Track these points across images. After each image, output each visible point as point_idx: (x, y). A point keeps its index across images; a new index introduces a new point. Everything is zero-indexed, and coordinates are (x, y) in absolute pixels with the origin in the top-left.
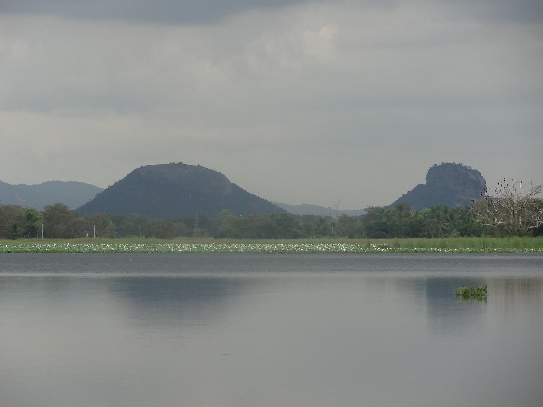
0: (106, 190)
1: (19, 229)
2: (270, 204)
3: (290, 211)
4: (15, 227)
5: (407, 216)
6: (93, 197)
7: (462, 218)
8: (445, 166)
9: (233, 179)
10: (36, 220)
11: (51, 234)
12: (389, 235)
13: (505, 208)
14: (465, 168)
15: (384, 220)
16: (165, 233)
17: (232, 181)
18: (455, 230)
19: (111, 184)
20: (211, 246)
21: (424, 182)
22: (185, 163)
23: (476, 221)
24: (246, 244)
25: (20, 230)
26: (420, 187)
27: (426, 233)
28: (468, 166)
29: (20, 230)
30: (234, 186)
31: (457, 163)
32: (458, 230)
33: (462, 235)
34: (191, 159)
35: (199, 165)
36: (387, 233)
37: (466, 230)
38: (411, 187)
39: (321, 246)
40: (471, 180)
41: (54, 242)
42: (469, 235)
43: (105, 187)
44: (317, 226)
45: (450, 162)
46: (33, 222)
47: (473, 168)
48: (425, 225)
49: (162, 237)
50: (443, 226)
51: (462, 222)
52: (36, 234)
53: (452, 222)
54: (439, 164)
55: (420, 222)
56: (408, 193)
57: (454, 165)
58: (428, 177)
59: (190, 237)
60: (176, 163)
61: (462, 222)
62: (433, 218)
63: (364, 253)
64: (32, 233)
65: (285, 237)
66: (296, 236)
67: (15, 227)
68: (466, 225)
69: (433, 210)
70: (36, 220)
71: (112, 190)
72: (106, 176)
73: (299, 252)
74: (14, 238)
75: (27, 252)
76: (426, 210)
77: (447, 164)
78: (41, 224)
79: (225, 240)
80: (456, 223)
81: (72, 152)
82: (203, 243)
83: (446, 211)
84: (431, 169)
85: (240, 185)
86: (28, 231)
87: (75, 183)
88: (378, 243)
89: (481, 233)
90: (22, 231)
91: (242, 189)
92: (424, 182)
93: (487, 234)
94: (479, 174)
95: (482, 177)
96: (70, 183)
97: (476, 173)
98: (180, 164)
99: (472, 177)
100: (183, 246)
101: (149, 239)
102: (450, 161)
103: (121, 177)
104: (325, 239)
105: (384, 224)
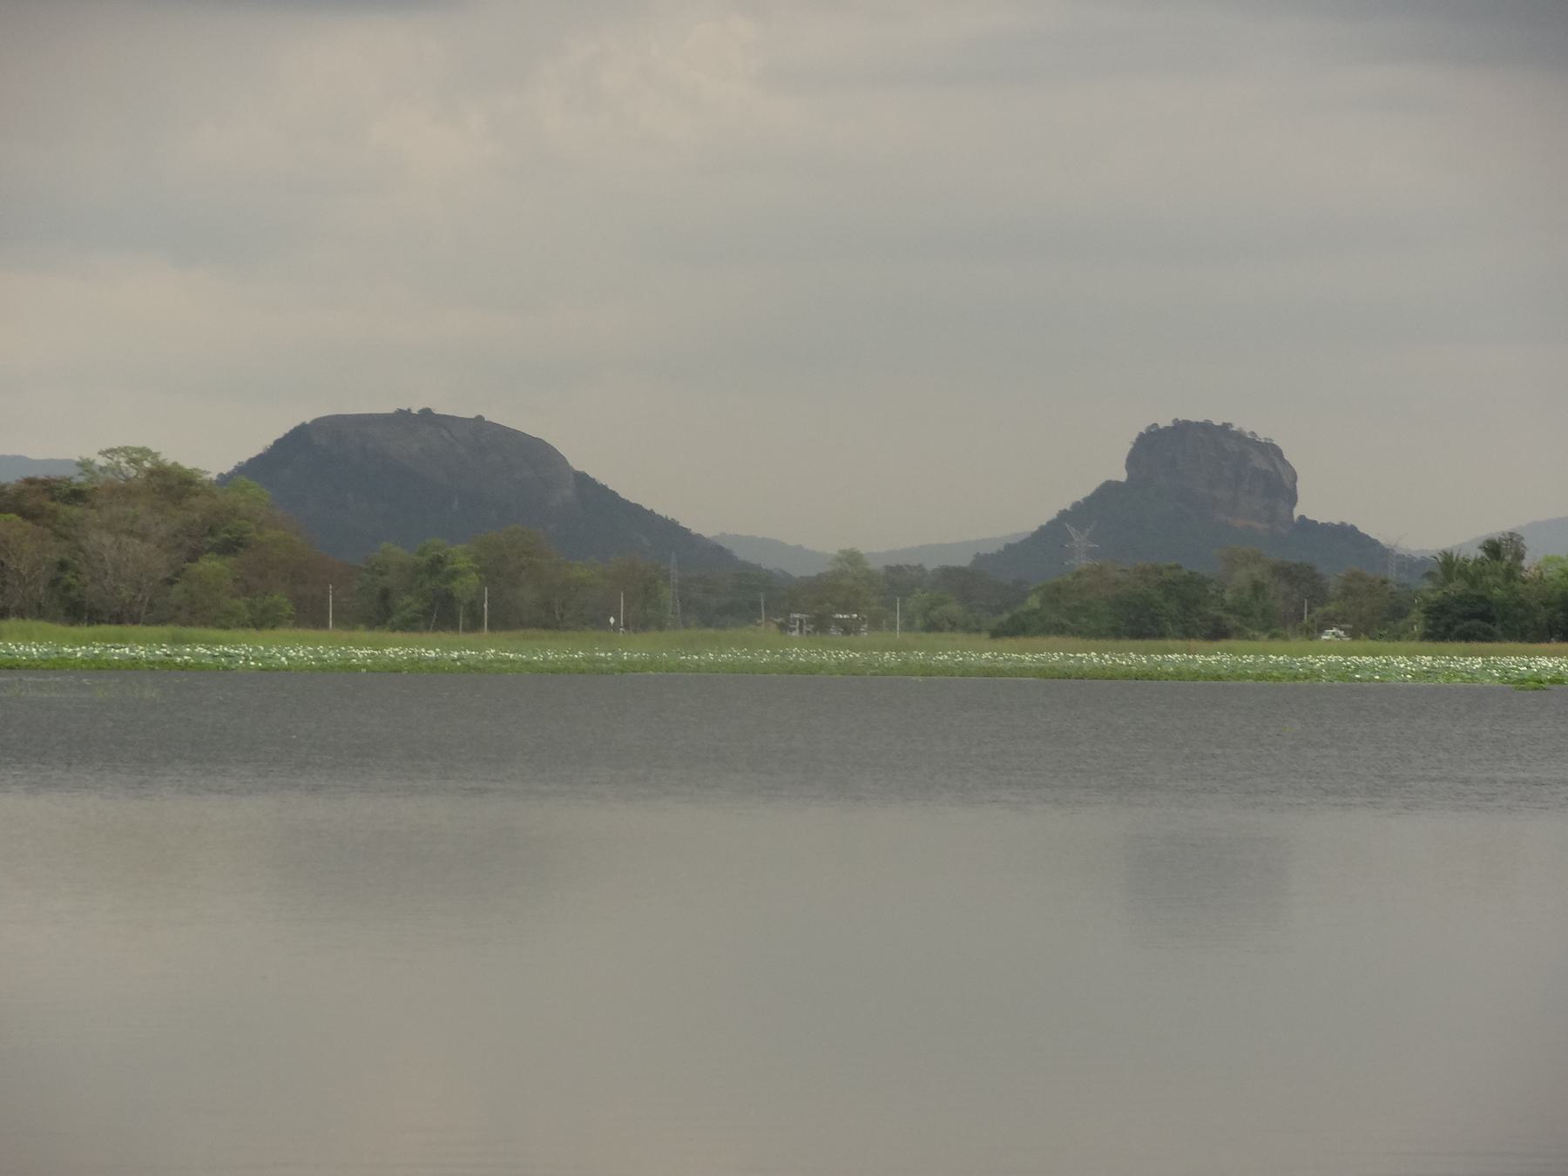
8: (1182, 429)
10: (454, 574)
14: (1239, 436)
17: (577, 463)
20: (987, 655)
21: (1122, 476)
22: (440, 410)
28: (1247, 430)
30: (583, 480)
31: (1217, 423)
40: (1257, 470)
44: (840, 598)
45: (1197, 416)
47: (1262, 436)
54: (1165, 422)
57: (1206, 427)
58: (1133, 461)
59: (326, 626)
60: (415, 411)
65: (1187, 634)
66: (1218, 633)
70: (454, 574)
77: (1187, 423)
78: (467, 585)
81: (132, 360)
82: (1022, 652)
84: (1142, 438)
91: (605, 487)
92: (1122, 476)
97: (1271, 451)
98: (426, 412)
99: (1259, 462)
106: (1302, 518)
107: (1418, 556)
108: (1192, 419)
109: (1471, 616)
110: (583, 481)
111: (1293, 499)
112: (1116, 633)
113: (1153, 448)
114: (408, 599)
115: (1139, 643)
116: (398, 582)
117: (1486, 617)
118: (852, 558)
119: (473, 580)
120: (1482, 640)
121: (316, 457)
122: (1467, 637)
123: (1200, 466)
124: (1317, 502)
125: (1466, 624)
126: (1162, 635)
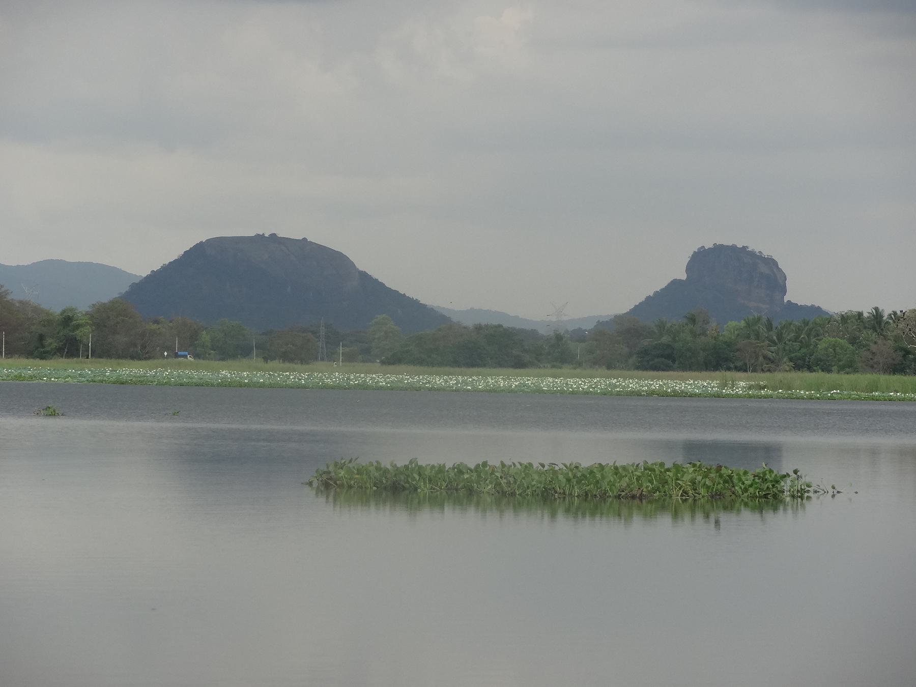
0: (148, 277)
1: (49, 341)
2: (424, 306)
3: (455, 319)
4: (41, 337)
5: (704, 333)
6: (125, 288)
7: (796, 339)
8: (719, 249)
9: (361, 265)
10: (78, 326)
11: (103, 351)
12: (676, 365)
13: (814, 322)
14: (752, 254)
15: (665, 339)
16: (231, 349)
17: (361, 266)
18: (785, 360)
19: (156, 267)
21: (683, 276)
22: (281, 234)
23: (822, 345)
24: (411, 374)
25: (51, 343)
26: (675, 283)
27: (739, 364)
29: (51, 343)
30: (364, 276)
31: (740, 246)
32: (791, 360)
33: (798, 367)
34: (291, 228)
35: (305, 239)
36: (674, 361)
37: (804, 360)
38: (661, 284)
39: (548, 382)
40: (764, 274)
41: (119, 364)
42: (810, 369)
43: (144, 272)
45: (728, 242)
46: (73, 331)
47: (766, 254)
48: (738, 350)
49: (292, 360)
50: (766, 352)
51: (797, 345)
52: (78, 350)
53: (780, 346)
54: (709, 245)
55: (729, 344)
56: (656, 293)
57: (733, 248)
58: (689, 268)
60: (267, 235)
61: (797, 345)
62: (748, 337)
63: (804, 399)
64: (70, 348)
65: (500, 364)
66: (519, 364)
67: (41, 337)
68: (803, 350)
69: (748, 325)
70: (78, 326)
71: (155, 277)
72: (142, 252)
73: (693, 395)
74: (43, 356)
75: (212, 385)
76: (733, 324)
78: (87, 335)
79: (403, 367)
80: (787, 348)
81: (90, 212)
83: (770, 327)
85: (370, 272)
86: (65, 344)
87: (89, 265)
88: (748, 379)
89: (831, 366)
90: (54, 345)
92: (683, 276)
93: (841, 369)
94: (775, 263)
95: (780, 270)
96: (79, 264)
97: (771, 263)
98: (273, 236)
99: (763, 269)
100: (333, 375)
101: (271, 364)
102: (727, 241)
103: (663, 286)
104: (566, 369)
105: (668, 346)
106: (789, 301)
107: (470, 323)
108: (725, 243)
109: (662, 356)
110: (365, 277)
111: (784, 291)
112: (456, 363)
113: (707, 261)
114: (50, 340)
115: (517, 371)
116: (247, 340)
117: (670, 357)
118: (500, 326)
119: (87, 329)
120: (663, 370)
121: (212, 263)
122: (655, 368)
123: (732, 271)
124: (799, 293)
125: (656, 360)
126: (484, 366)
